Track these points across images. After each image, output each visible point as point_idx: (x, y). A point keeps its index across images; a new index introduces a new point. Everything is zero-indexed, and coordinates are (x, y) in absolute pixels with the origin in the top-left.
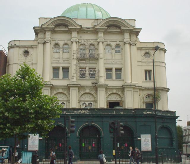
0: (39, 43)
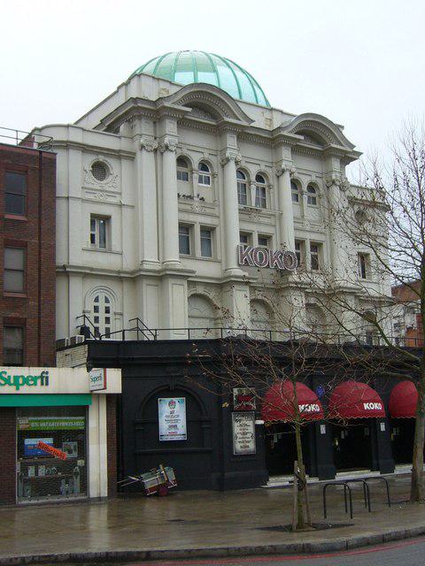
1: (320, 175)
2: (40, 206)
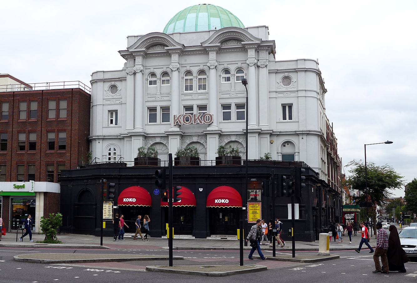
0: (128, 74)
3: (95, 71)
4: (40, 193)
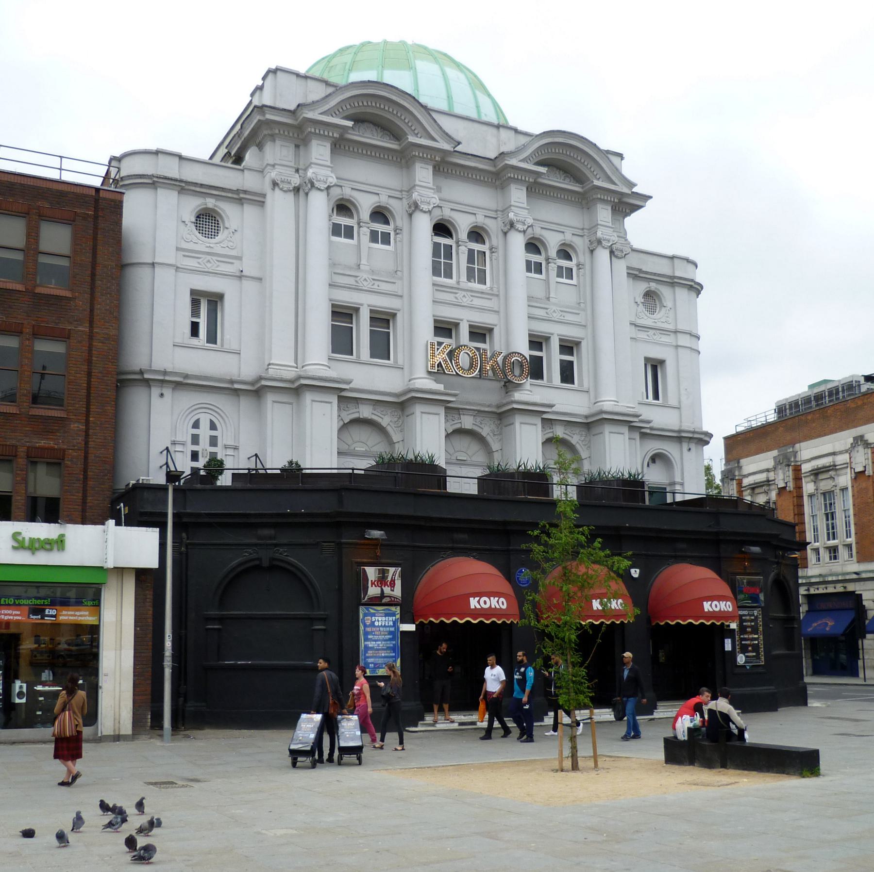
1: (580, 232)
2: (93, 275)
3: (691, 258)
4: (120, 571)
